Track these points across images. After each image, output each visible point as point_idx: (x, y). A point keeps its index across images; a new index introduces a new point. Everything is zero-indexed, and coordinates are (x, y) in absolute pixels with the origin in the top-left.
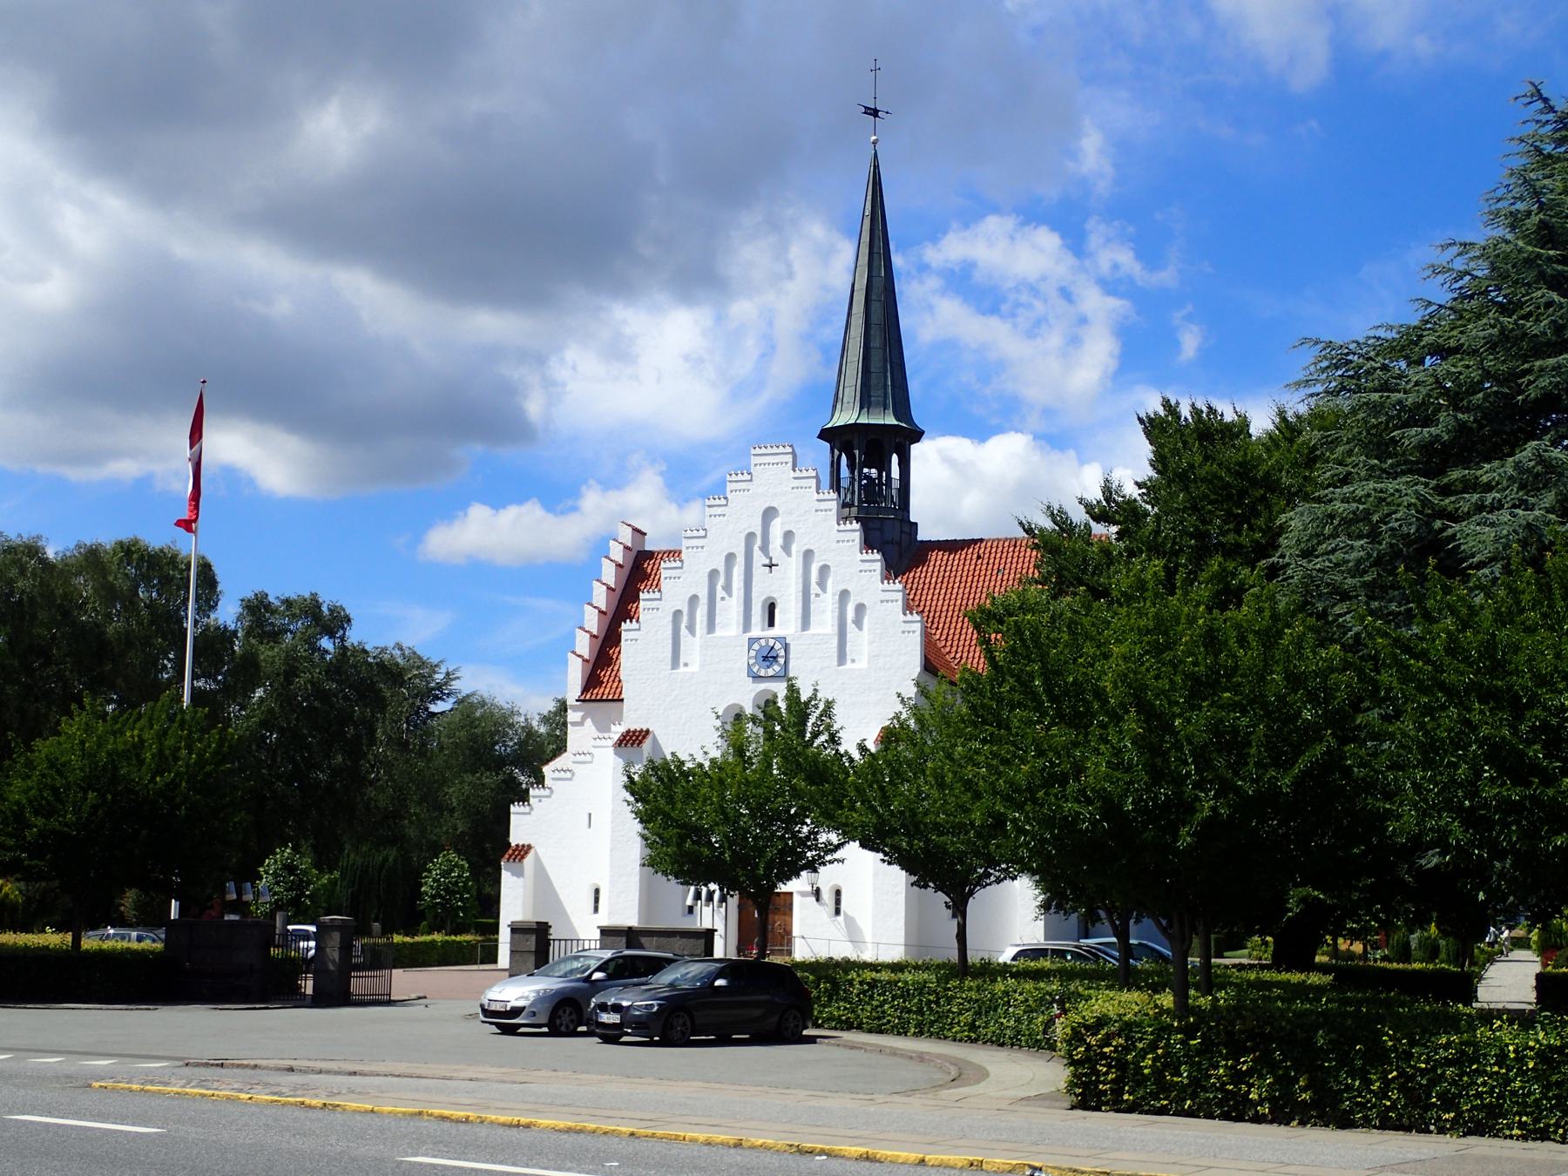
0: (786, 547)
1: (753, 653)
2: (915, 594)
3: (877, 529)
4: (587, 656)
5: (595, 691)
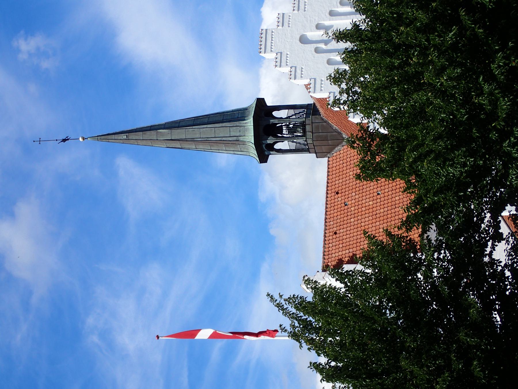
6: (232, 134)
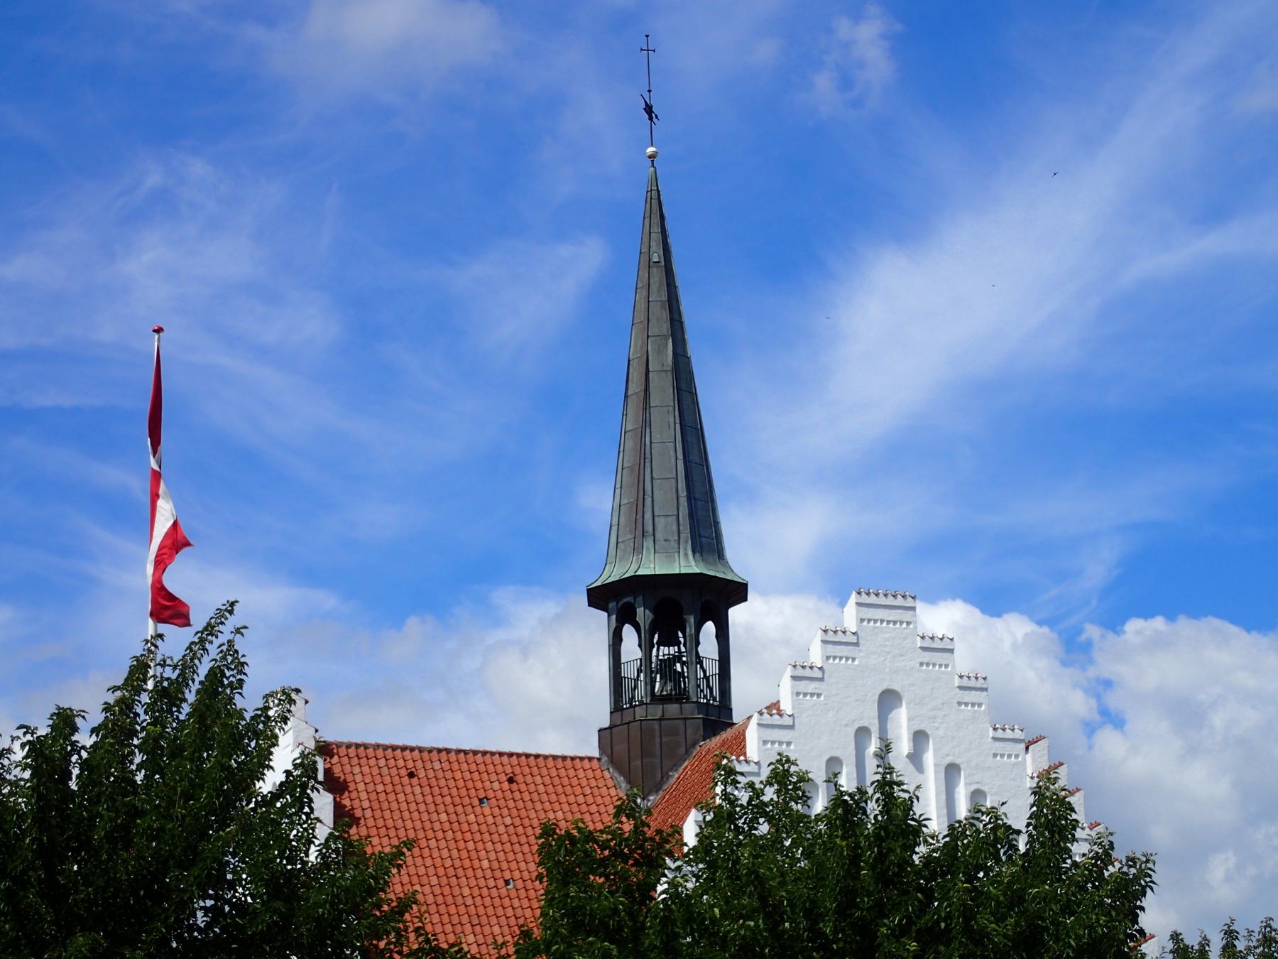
0: (915, 758)
6: (660, 522)
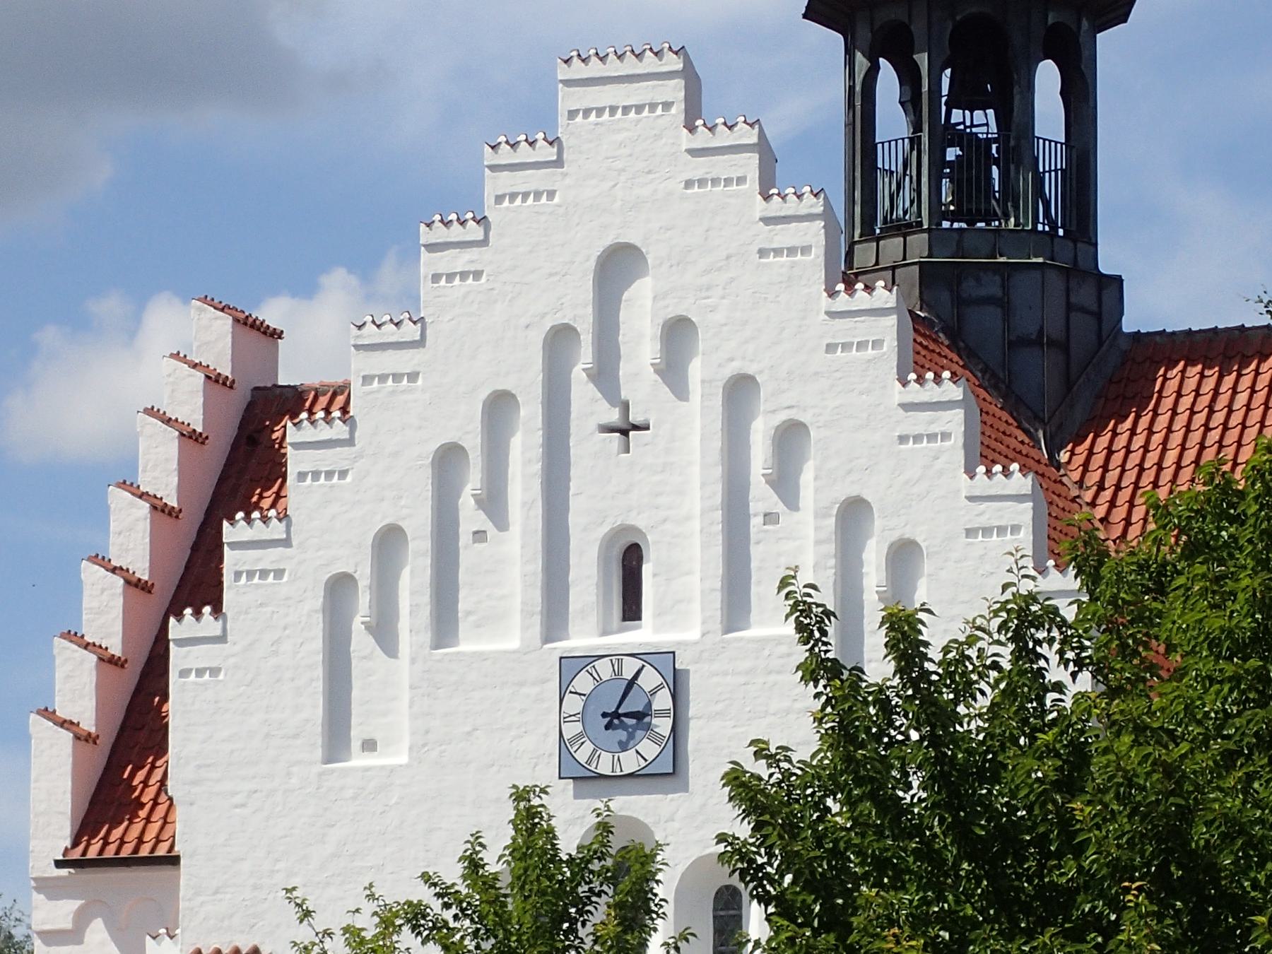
1: (574, 704)
2: (1112, 504)
3: (989, 300)
4: (88, 724)
5: (117, 833)
